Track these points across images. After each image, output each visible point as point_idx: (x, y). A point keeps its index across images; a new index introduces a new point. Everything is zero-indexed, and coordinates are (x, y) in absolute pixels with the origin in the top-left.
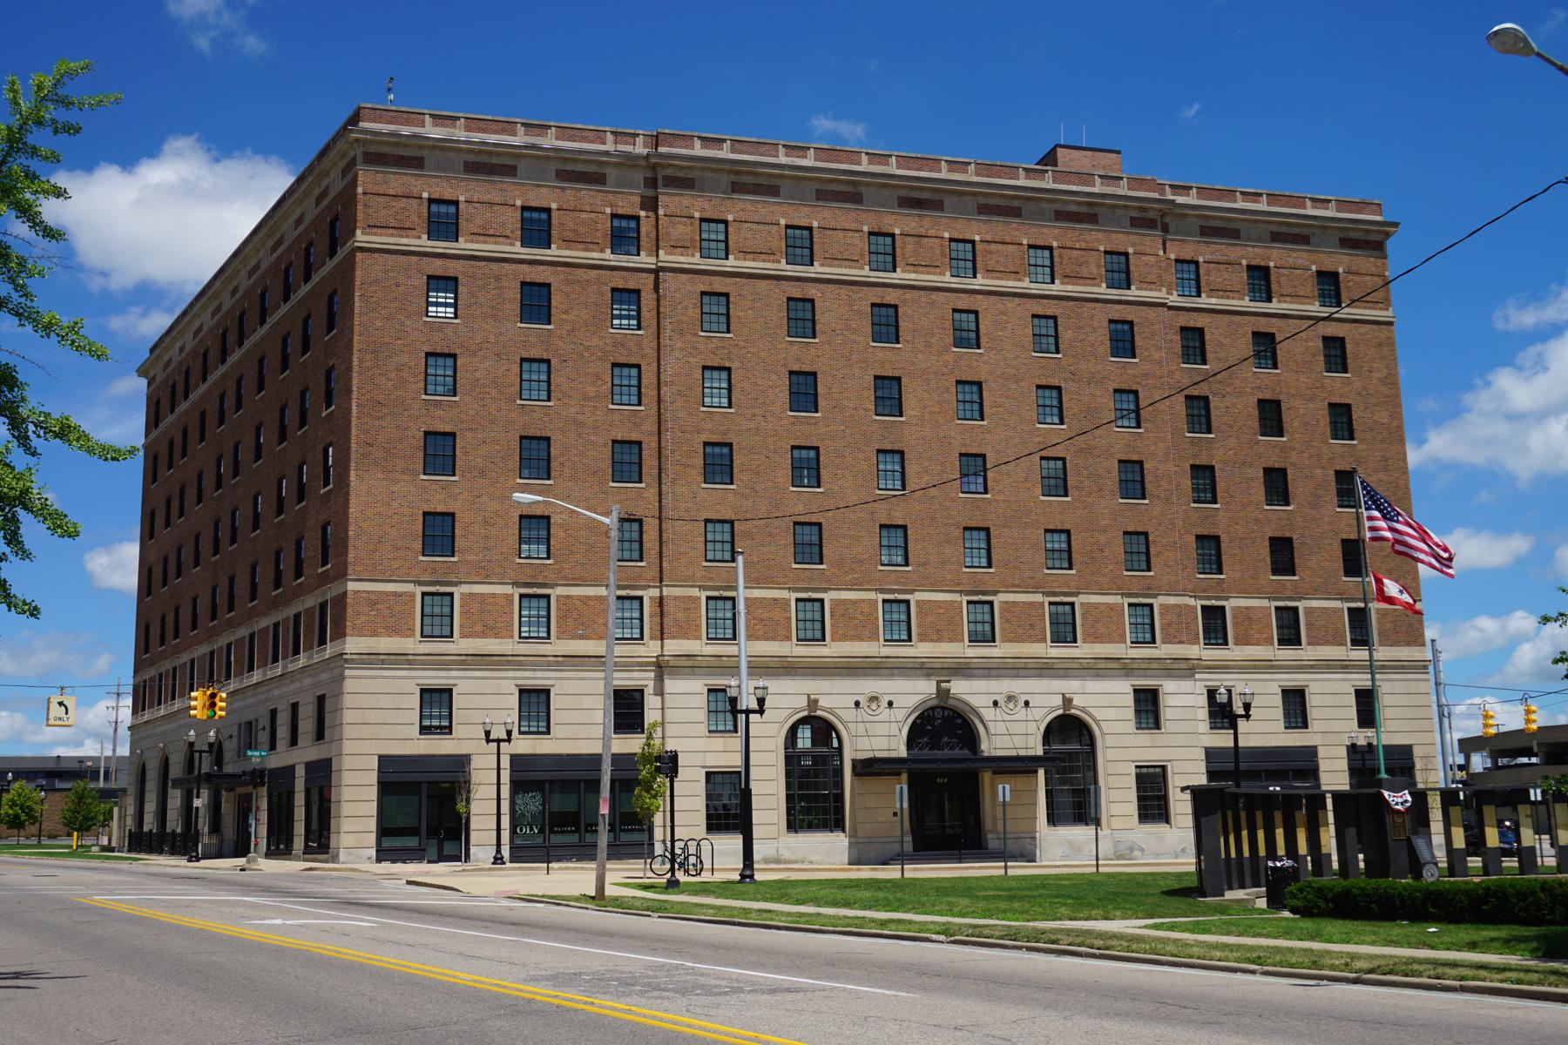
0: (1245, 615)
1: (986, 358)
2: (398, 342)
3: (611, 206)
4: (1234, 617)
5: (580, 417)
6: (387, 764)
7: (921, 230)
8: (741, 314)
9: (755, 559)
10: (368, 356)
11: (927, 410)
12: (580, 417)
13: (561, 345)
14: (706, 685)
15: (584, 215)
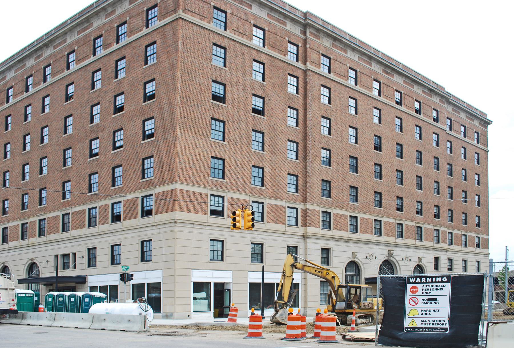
0: (428, 230)
1: (403, 137)
2: (200, 71)
3: (288, 37)
4: (406, 228)
5: (276, 126)
6: (215, 317)
7: (388, 83)
8: (335, 98)
9: (338, 198)
10: (186, 74)
11: (388, 151)
12: (276, 126)
13: (269, 92)
14: (321, 246)
15: (278, 37)
